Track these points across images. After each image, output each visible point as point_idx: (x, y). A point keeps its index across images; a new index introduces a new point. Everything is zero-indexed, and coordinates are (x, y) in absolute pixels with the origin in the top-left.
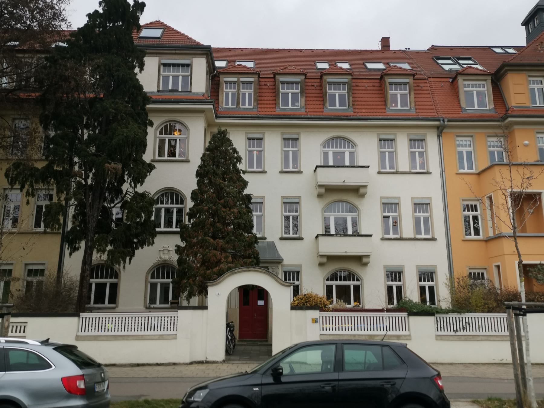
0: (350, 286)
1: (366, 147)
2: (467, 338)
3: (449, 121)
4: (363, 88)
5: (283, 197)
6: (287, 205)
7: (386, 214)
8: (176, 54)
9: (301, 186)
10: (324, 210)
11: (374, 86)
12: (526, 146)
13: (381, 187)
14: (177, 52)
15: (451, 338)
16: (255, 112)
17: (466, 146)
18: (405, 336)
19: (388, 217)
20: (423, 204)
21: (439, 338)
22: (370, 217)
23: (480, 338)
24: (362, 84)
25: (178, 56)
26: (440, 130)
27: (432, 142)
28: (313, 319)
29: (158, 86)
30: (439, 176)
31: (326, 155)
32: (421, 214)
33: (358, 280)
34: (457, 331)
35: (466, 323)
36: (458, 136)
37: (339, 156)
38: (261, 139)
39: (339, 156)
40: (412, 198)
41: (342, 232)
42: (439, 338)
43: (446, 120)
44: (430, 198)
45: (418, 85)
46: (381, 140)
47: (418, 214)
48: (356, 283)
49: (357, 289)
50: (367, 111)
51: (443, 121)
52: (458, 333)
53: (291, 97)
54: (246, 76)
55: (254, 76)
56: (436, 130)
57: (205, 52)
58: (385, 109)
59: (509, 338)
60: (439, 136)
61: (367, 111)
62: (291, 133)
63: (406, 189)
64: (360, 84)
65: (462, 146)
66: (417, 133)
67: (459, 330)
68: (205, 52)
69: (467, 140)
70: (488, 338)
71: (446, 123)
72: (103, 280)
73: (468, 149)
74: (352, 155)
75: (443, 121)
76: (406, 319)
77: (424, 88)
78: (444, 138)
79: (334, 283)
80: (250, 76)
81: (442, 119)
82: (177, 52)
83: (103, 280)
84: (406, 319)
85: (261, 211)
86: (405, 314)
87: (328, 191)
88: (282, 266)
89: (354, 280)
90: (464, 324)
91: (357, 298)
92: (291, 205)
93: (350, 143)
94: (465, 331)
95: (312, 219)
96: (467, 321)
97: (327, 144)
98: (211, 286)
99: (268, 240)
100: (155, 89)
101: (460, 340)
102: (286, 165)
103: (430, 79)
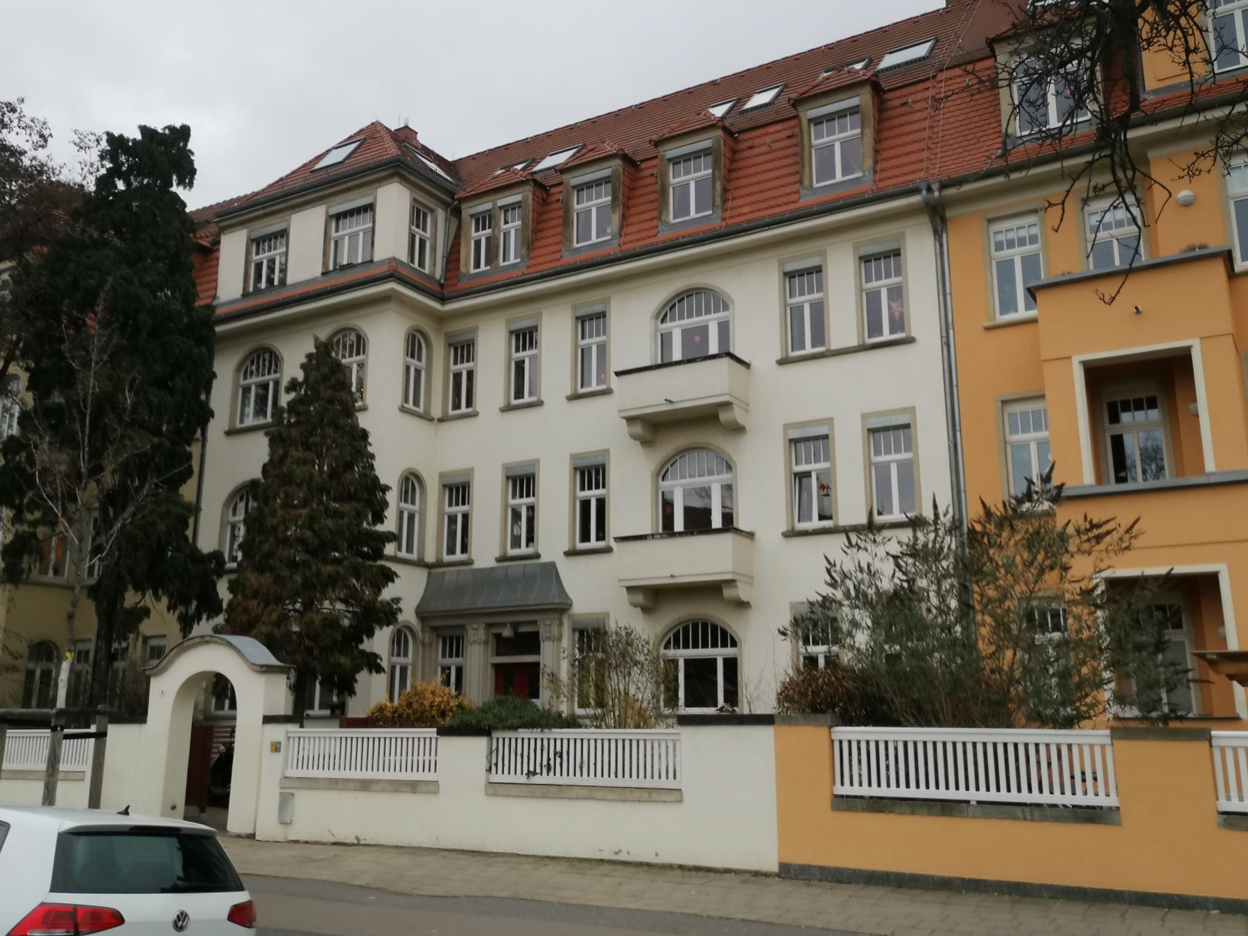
0: (715, 660)
1: (753, 301)
2: (559, 792)
3: (944, 186)
4: (763, 149)
5: (865, 417)
6: (881, 435)
7: (803, 468)
8: (349, 189)
9: (599, 427)
10: (662, 473)
11: (750, 148)
12: (1187, 204)
13: (781, 396)
14: (349, 185)
15: (515, 790)
16: (717, 223)
17: (1022, 242)
18: (427, 783)
19: (807, 474)
20: (807, 439)
21: (494, 789)
22: (759, 483)
23: (573, 793)
24: (762, 140)
25: (355, 192)
26: (937, 215)
27: (920, 251)
28: (272, 744)
29: (325, 263)
30: (936, 342)
31: (665, 340)
32: (893, 457)
33: (734, 644)
34: (534, 773)
35: (555, 753)
36: (990, 221)
37: (694, 338)
38: (818, 270)
39: (694, 338)
40: (865, 417)
41: (698, 521)
42: (491, 791)
43: (935, 187)
44: (912, 410)
45: (904, 100)
46: (865, 259)
47: (883, 458)
48: (729, 651)
49: (732, 666)
50: (754, 207)
51: (929, 189)
52: (536, 779)
53: (593, 216)
54: (507, 193)
55: (522, 189)
56: (925, 219)
57: (391, 171)
58: (797, 192)
59: (43, 776)
60: (937, 234)
61: (754, 207)
62: (589, 302)
63: (846, 394)
64: (757, 142)
65: (1011, 244)
66: (876, 239)
67: (538, 770)
68: (391, 171)
69: (1027, 226)
70: (591, 793)
71: (936, 194)
72: (708, 652)
73: (1029, 249)
74: (724, 328)
75: (929, 189)
76: (434, 741)
77: (919, 106)
78: (955, 237)
79: (682, 654)
80: (515, 191)
81: (923, 186)
82: (349, 185)
83: (708, 652)
84: (434, 741)
85: (827, 458)
86: (432, 731)
87: (653, 427)
88: (570, 617)
89: (724, 645)
90: (552, 756)
91: (732, 696)
92: (901, 432)
93: (719, 302)
94: (552, 773)
95: (631, 502)
96: (558, 749)
97: (667, 311)
98: (156, 675)
99: (544, 559)
100: (318, 271)
101: (544, 797)
102: (798, 342)
103: (941, 76)
